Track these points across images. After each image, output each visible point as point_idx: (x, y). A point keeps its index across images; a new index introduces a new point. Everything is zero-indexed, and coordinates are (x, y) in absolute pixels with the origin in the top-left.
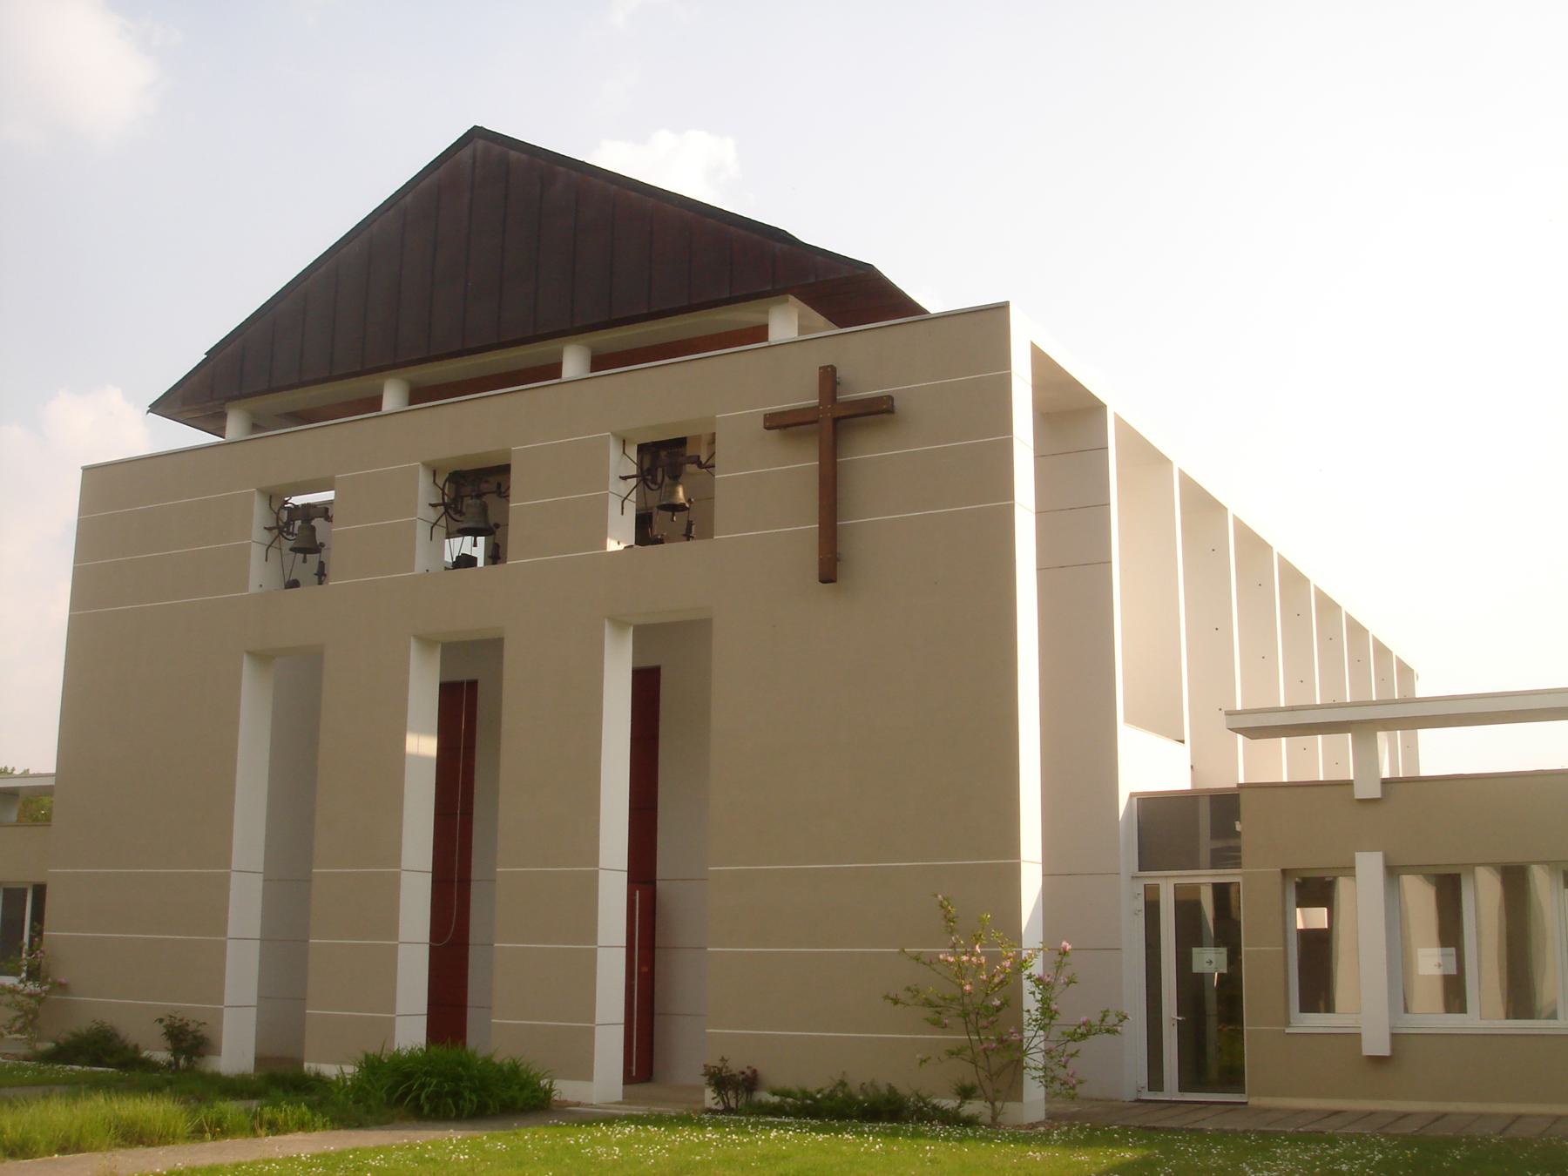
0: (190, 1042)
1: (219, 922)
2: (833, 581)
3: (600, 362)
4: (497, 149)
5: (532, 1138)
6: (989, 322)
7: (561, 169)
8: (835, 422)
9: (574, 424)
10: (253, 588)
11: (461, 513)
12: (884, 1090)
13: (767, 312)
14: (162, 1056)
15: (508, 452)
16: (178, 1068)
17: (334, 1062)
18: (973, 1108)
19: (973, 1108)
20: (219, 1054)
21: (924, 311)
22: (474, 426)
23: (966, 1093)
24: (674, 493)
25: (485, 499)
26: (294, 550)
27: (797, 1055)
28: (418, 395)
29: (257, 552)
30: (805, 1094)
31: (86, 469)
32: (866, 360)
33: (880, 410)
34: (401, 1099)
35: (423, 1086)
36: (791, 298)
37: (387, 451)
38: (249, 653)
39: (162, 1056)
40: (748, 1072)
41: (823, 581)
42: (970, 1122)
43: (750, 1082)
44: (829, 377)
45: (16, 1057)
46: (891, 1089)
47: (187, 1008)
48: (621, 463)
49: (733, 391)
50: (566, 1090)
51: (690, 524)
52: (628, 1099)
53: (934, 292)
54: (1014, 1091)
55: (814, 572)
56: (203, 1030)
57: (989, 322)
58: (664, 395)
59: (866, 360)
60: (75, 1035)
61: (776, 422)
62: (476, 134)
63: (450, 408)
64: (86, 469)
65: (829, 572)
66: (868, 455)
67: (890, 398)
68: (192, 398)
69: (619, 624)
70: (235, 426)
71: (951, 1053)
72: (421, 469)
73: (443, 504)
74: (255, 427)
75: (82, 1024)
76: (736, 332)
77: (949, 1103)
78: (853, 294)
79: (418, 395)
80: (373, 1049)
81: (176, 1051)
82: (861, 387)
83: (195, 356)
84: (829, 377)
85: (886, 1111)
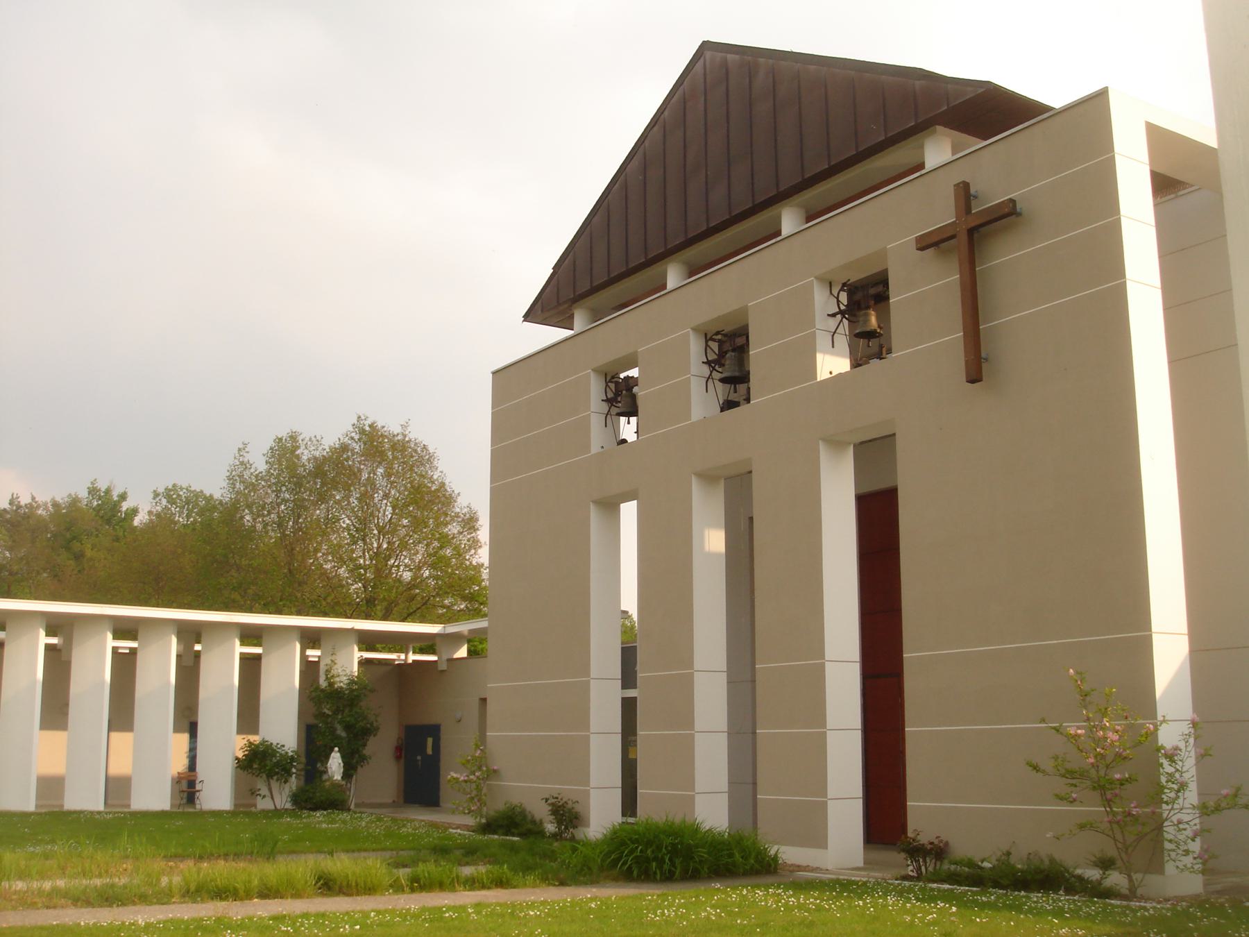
0: (568, 816)
1: (583, 721)
2: (979, 380)
4: (719, 55)
5: (762, 897)
6: (1094, 107)
7: (762, 60)
8: (975, 232)
9: (787, 276)
10: (595, 449)
11: (722, 365)
13: (922, 147)
14: (550, 827)
16: (530, 842)
18: (1115, 879)
20: (588, 826)
21: (1052, 109)
23: (1106, 864)
24: (867, 321)
26: (723, 380)
28: (693, 270)
29: (697, 386)
30: (971, 864)
32: (996, 169)
33: (1007, 214)
34: (614, 864)
35: (632, 852)
36: (938, 128)
37: (667, 324)
38: (595, 502)
40: (936, 842)
41: (972, 381)
42: (1107, 894)
44: (964, 193)
45: (467, 828)
46: (1052, 861)
47: (566, 790)
48: (823, 303)
49: (887, 225)
50: (789, 854)
51: (881, 347)
52: (869, 864)
53: (1051, 88)
54: (1155, 863)
56: (578, 808)
57: (1094, 107)
59: (996, 169)
61: (925, 243)
65: (974, 377)
66: (1007, 258)
67: (1012, 201)
68: (541, 311)
69: (836, 444)
70: (580, 321)
71: (1082, 827)
72: (592, 374)
73: (841, 312)
75: (497, 806)
77: (1093, 874)
78: (988, 112)
79: (693, 270)
81: (559, 822)
82: (992, 193)
83: (544, 273)
84: (964, 193)
85: (1045, 879)
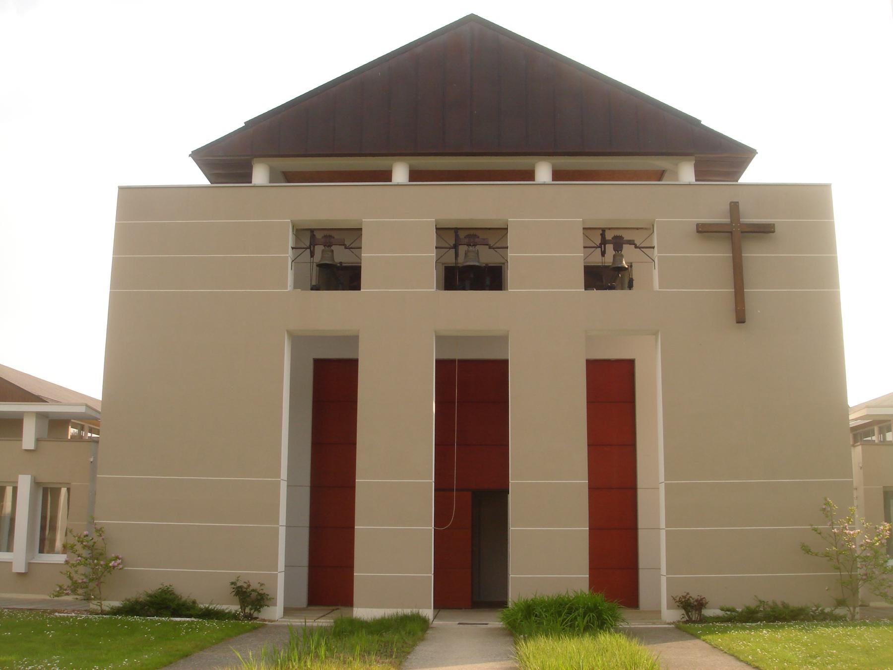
3: (558, 175)
9: (542, 214)
12: (770, 603)
13: (677, 165)
14: (235, 608)
15: (361, 223)
17: (408, 608)
18: (840, 611)
19: (840, 611)
22: (472, 203)
25: (333, 248)
27: (722, 590)
31: (122, 189)
39: (235, 608)
43: (700, 604)
55: (733, 317)
58: (610, 202)
60: (150, 596)
61: (704, 230)
62: (472, 20)
63: (438, 187)
64: (122, 189)
65: (741, 319)
66: (755, 254)
74: (272, 179)
75: (140, 591)
76: (514, 171)
80: (198, 602)
83: (238, 123)
